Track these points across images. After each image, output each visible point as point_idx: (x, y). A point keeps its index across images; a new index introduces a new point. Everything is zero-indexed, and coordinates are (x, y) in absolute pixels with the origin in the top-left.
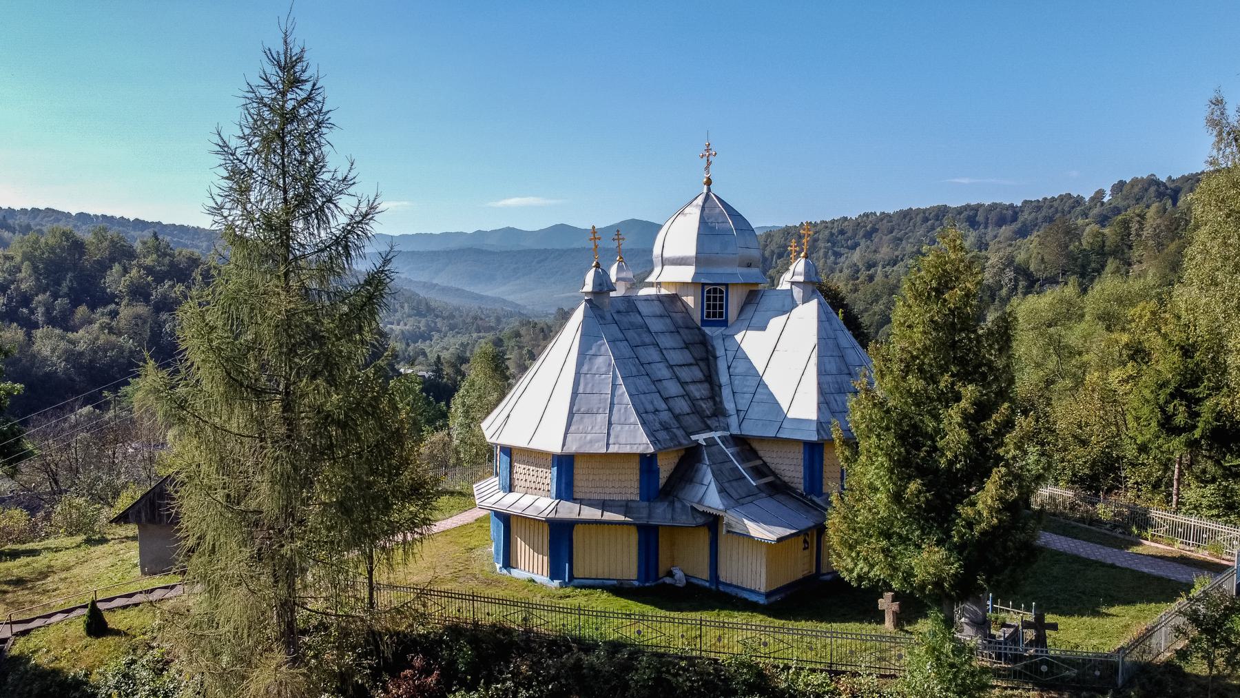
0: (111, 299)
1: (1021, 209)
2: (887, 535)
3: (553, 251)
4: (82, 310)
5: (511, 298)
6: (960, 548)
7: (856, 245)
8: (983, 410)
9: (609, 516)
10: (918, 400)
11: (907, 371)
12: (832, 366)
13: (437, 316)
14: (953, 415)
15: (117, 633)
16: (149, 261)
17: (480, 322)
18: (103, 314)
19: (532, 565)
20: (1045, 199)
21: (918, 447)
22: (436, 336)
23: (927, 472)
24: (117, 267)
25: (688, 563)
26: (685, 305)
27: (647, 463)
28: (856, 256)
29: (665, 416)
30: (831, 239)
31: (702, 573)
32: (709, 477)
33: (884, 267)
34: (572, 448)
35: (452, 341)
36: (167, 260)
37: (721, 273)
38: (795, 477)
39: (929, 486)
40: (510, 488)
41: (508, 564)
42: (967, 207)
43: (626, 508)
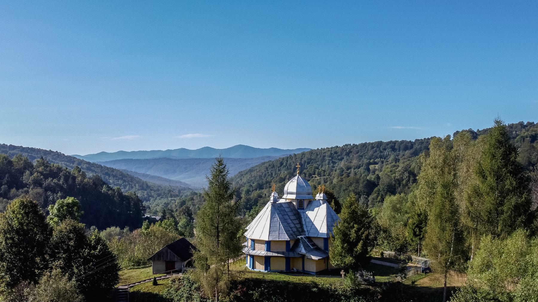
0: (25, 185)
1: (415, 143)
2: (341, 256)
3: (203, 159)
4: (13, 191)
5: (183, 181)
6: (354, 258)
7: (343, 158)
8: (359, 230)
9: (279, 255)
10: (347, 228)
11: (344, 222)
12: (330, 220)
13: (151, 190)
14: (353, 231)
15: (159, 285)
16: (40, 169)
17: (172, 193)
18: (22, 192)
19: (260, 268)
20: (425, 139)
21: (347, 237)
22: (152, 199)
23: (348, 242)
24: (28, 172)
25: (298, 266)
26: (293, 204)
27: (287, 242)
28: (342, 164)
29: (291, 232)
30: (331, 156)
31: (301, 269)
32: (302, 246)
33: (354, 169)
34: (271, 239)
35: (159, 201)
36: (48, 169)
37: (302, 197)
38: (320, 245)
39: (348, 245)
40: (254, 249)
41: (253, 268)
42: (391, 142)
43: (283, 253)
